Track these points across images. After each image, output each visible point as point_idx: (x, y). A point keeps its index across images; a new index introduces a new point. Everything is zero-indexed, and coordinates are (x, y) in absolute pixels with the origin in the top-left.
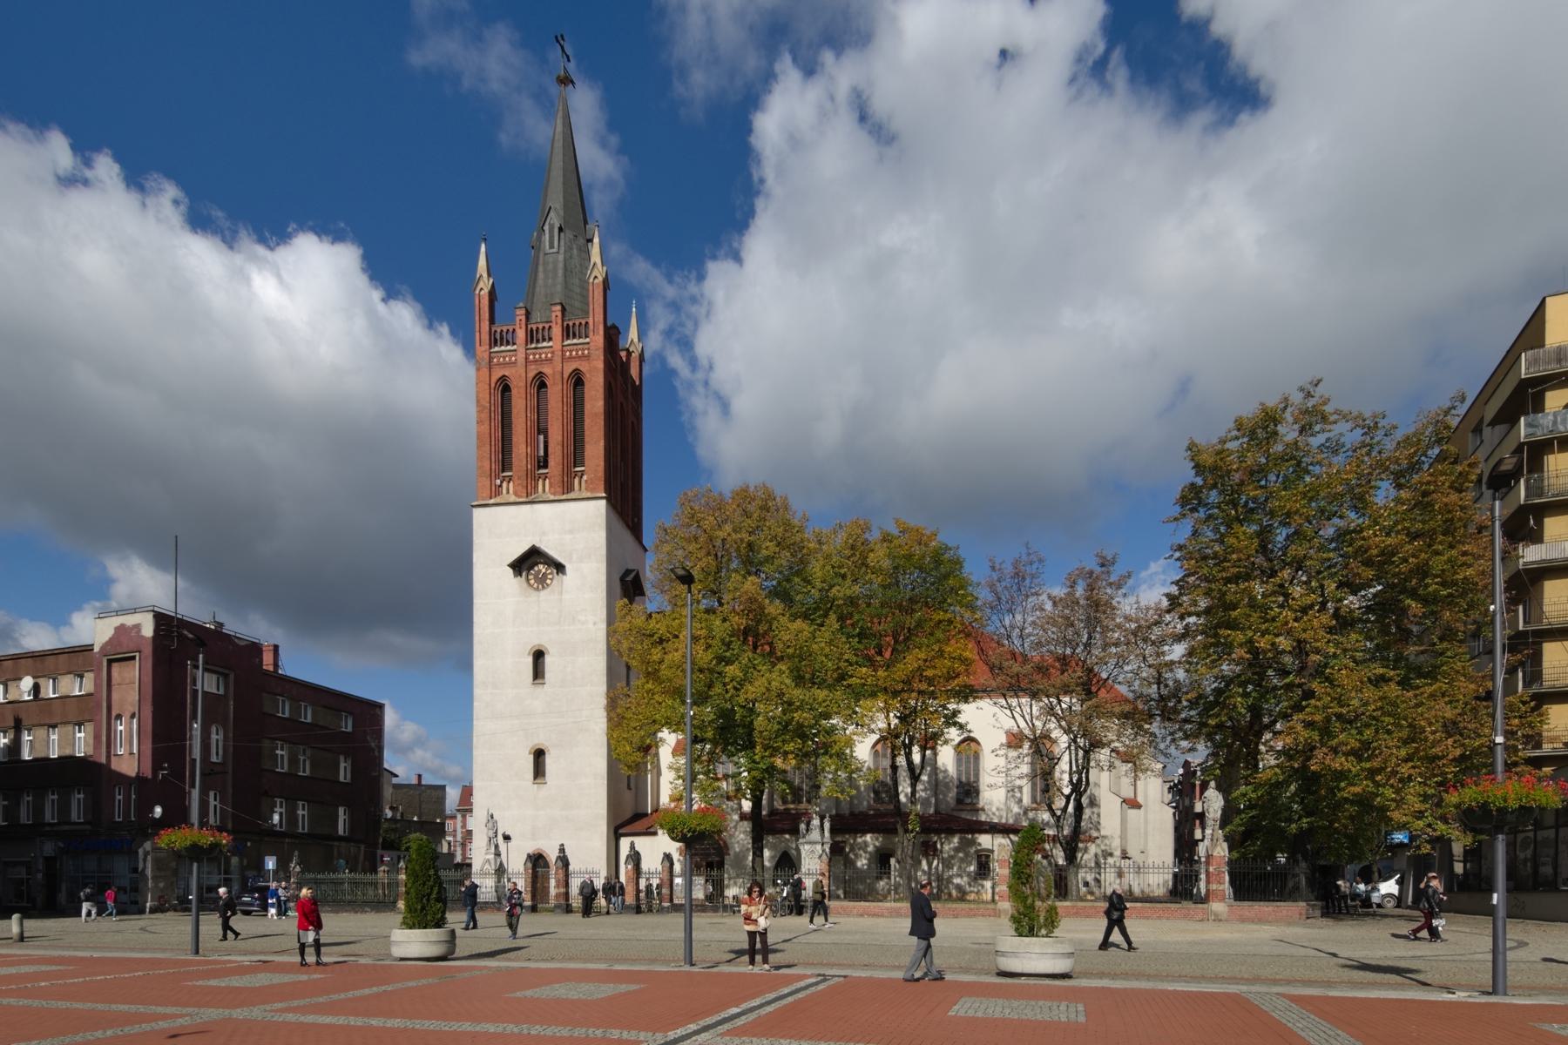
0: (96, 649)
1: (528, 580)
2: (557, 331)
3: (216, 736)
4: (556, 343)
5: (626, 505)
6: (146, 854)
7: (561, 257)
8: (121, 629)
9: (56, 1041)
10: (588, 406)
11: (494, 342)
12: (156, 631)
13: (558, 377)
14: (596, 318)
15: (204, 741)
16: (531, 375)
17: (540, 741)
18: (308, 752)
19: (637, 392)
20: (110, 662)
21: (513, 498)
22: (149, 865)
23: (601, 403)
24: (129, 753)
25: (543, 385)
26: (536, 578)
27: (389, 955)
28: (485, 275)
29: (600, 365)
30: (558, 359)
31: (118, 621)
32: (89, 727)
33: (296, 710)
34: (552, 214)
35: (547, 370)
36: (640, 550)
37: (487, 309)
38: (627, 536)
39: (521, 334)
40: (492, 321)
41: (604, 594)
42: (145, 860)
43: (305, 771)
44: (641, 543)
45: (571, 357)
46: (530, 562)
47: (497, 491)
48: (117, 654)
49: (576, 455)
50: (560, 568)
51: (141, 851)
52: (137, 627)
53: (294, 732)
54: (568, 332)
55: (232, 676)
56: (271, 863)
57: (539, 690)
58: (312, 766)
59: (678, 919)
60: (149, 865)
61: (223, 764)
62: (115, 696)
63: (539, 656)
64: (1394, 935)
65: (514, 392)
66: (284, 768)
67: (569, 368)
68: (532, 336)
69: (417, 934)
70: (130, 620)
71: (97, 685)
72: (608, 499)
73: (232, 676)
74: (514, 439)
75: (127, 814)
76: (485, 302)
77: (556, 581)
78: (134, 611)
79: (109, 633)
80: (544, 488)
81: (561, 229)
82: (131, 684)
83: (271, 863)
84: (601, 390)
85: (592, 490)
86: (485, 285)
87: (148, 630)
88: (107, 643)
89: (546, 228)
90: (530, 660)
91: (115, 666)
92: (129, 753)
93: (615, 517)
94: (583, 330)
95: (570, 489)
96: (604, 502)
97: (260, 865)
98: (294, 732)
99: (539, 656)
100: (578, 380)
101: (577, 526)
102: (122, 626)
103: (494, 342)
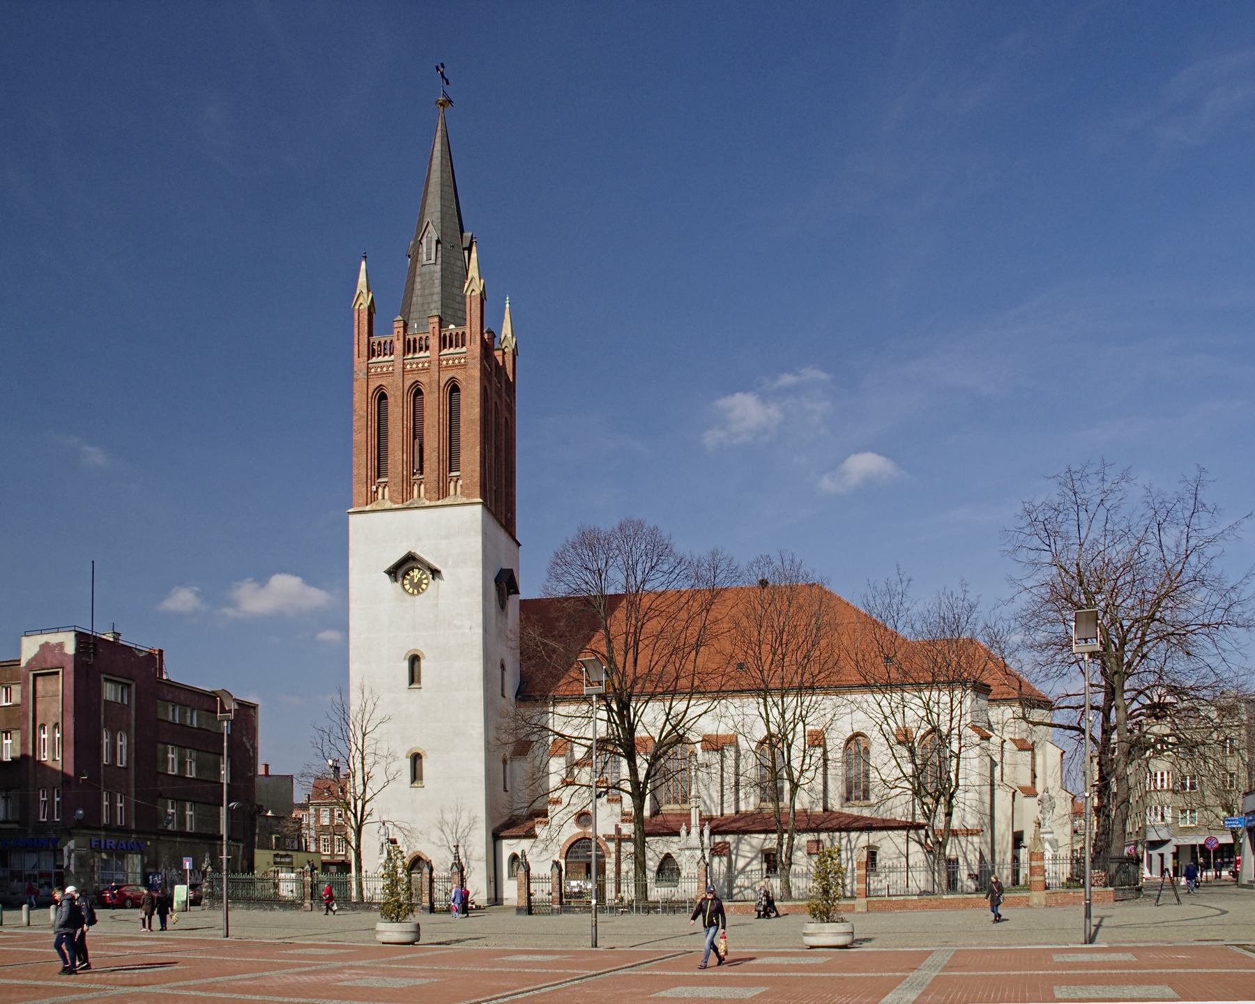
0: (23, 664)
1: (403, 585)
2: (434, 342)
3: (122, 742)
4: (432, 353)
5: (499, 500)
6: (70, 852)
7: (438, 268)
8: (45, 647)
9: (47, 1001)
10: (463, 413)
11: (372, 353)
12: (76, 649)
13: (435, 386)
14: (472, 328)
15: (118, 748)
16: (408, 383)
17: (418, 746)
18: (194, 755)
19: (511, 387)
20: (35, 676)
21: (388, 505)
22: (72, 862)
23: (477, 410)
24: (53, 752)
25: (419, 392)
26: (412, 584)
27: (375, 941)
28: (365, 291)
29: (477, 373)
30: (435, 368)
31: (42, 639)
32: (17, 735)
33: (183, 715)
34: (431, 227)
35: (423, 379)
36: (514, 545)
37: (366, 323)
38: (502, 536)
39: (399, 346)
40: (370, 334)
41: (480, 598)
42: (69, 857)
43: (191, 773)
44: (514, 538)
45: (376, 374)
46: (403, 568)
47: (372, 497)
48: (43, 669)
49: (452, 460)
50: (435, 573)
51: (65, 849)
52: (61, 645)
53: (185, 737)
54: (444, 342)
55: (134, 686)
56: (188, 865)
57: (415, 693)
58: (198, 768)
59: (587, 918)
60: (72, 862)
61: (125, 768)
62: (39, 707)
63: (414, 660)
64: (870, 940)
65: (391, 400)
66: (173, 770)
67: (445, 377)
68: (410, 347)
69: (395, 926)
70: (53, 639)
71: (24, 696)
72: (484, 504)
73: (134, 686)
74: (390, 446)
75: (51, 815)
76: (365, 316)
77: (432, 586)
78: (58, 630)
79: (36, 650)
80: (385, 498)
81: (438, 242)
82: (55, 696)
83: (188, 865)
84: (478, 398)
85: (468, 496)
86: (364, 301)
87: (70, 649)
88: (33, 659)
89: (424, 241)
90: (406, 664)
91: (39, 679)
92: (53, 752)
93: (491, 519)
94: (460, 340)
95: (445, 494)
96: (480, 507)
97: (180, 865)
98: (185, 737)
99: (414, 660)
100: (454, 388)
101: (453, 530)
102: (47, 643)
103: (372, 353)
